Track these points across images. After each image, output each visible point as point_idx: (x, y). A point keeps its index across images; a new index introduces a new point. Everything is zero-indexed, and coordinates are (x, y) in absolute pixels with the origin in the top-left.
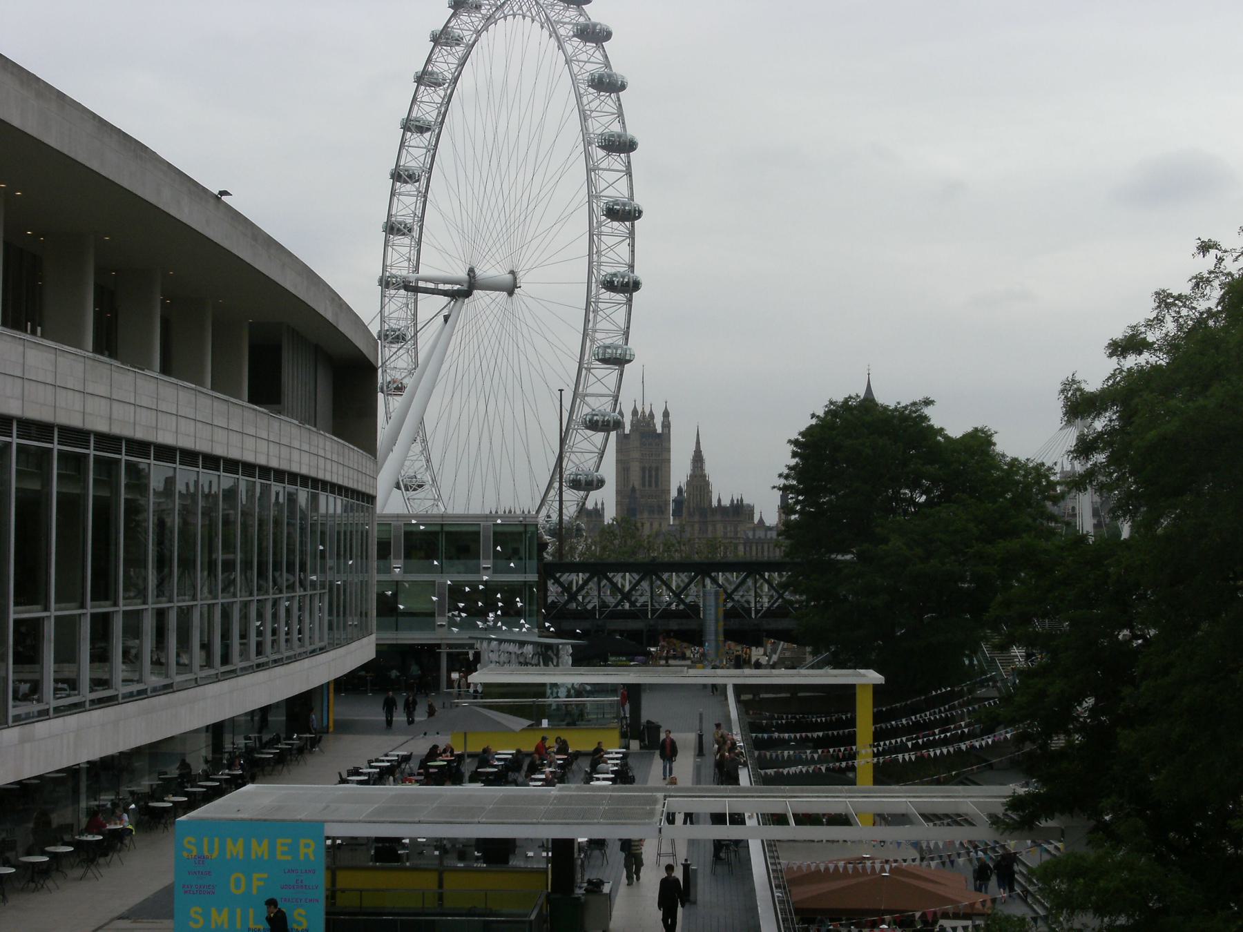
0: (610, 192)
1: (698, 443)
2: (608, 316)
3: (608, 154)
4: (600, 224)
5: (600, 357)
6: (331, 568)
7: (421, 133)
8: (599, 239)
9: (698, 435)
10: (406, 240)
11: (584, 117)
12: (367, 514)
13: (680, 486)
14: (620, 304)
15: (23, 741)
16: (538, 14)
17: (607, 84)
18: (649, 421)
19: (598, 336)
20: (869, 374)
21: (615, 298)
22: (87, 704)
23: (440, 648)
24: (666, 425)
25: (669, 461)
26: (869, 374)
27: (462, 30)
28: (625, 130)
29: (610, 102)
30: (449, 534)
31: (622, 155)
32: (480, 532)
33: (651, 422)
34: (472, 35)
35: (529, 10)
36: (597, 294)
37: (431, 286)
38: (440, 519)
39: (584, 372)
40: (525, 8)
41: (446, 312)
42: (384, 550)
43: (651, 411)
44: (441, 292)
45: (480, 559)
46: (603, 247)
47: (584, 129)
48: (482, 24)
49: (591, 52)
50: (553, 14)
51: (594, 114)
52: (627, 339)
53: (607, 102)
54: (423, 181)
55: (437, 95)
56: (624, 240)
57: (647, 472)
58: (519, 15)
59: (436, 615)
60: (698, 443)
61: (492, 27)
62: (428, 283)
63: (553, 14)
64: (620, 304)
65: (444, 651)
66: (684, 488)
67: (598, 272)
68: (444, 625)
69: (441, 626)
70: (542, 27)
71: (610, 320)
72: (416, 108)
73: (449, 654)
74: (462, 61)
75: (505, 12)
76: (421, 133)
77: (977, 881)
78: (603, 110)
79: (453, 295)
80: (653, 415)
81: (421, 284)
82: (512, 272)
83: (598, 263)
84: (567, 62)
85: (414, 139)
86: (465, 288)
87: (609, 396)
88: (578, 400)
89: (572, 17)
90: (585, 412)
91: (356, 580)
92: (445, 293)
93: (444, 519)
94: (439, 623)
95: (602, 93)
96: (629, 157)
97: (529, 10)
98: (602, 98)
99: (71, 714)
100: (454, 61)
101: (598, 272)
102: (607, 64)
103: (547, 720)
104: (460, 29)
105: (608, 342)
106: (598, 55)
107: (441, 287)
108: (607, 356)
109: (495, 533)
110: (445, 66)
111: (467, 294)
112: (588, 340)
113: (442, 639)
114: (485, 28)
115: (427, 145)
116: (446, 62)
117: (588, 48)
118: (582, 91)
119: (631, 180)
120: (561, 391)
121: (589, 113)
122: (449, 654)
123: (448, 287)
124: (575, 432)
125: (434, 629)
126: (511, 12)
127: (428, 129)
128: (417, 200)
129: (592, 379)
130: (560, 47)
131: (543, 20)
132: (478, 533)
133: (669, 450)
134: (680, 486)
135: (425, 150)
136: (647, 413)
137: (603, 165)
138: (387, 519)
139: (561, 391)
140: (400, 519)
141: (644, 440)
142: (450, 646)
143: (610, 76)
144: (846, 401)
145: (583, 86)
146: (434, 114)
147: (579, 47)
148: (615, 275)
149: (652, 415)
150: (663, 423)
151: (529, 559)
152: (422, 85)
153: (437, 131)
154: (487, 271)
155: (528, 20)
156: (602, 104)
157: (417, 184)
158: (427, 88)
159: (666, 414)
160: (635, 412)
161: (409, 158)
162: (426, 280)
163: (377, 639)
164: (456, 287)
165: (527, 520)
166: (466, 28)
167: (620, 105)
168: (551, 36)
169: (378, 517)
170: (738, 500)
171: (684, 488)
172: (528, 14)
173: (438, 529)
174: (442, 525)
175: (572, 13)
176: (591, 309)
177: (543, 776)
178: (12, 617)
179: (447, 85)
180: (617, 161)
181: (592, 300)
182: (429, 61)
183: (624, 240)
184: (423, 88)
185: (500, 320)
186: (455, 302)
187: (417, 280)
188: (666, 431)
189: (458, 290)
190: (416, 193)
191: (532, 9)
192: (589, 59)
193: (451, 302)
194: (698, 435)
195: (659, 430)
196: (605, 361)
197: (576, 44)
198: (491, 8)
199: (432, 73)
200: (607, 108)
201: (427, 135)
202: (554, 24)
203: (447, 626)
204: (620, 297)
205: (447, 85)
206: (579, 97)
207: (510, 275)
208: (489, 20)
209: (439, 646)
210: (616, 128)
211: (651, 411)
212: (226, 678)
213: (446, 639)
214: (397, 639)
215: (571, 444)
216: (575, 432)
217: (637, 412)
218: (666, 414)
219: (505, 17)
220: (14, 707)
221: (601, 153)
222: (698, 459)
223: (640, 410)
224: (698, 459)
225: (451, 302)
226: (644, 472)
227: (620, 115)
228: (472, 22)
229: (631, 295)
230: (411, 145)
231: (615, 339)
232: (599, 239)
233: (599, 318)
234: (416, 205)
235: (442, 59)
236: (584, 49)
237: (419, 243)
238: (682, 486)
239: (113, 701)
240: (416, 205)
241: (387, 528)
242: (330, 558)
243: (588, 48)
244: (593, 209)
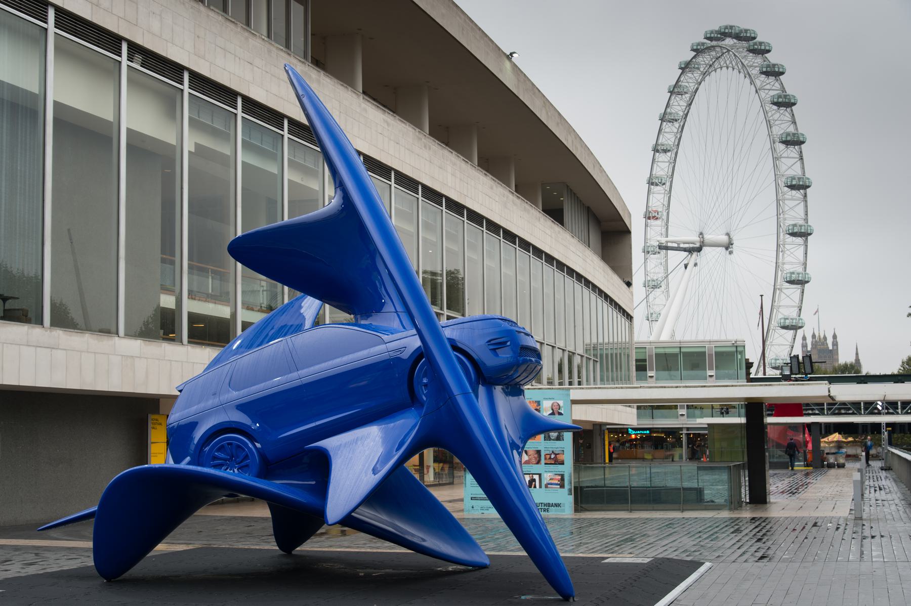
0: (791, 173)
2: (792, 253)
3: (787, 147)
4: (784, 194)
5: (788, 280)
7: (665, 152)
8: (784, 203)
9: (857, 349)
10: (658, 222)
11: (770, 125)
14: (800, 245)
16: (737, 64)
17: (785, 103)
18: (823, 342)
19: (786, 267)
21: (796, 241)
24: (835, 344)
27: (688, 82)
28: (797, 129)
29: (787, 114)
30: (686, 355)
31: (796, 147)
32: (706, 352)
33: (825, 342)
34: (695, 85)
35: (731, 62)
36: (784, 240)
37: (676, 245)
39: (778, 292)
40: (728, 62)
41: (686, 262)
42: (641, 367)
43: (825, 335)
44: (682, 249)
45: (706, 370)
46: (787, 208)
48: (701, 78)
50: (747, 62)
51: (777, 123)
52: (805, 268)
53: (784, 113)
54: (668, 184)
55: (673, 128)
56: (800, 203)
58: (725, 67)
59: (679, 408)
60: (857, 354)
61: (707, 78)
62: (673, 244)
63: (747, 62)
64: (800, 245)
67: (784, 225)
68: (684, 415)
69: (682, 415)
70: (740, 72)
71: (793, 256)
72: (661, 136)
73: (688, 435)
74: (689, 103)
75: (716, 67)
76: (665, 152)
79: (690, 251)
80: (826, 338)
81: (670, 245)
82: (728, 234)
83: (783, 218)
84: (757, 91)
85: (661, 157)
86: (698, 245)
87: (795, 307)
88: (775, 311)
90: (779, 317)
92: (685, 250)
93: (681, 344)
94: (681, 413)
96: (800, 148)
97: (731, 62)
98: (782, 112)
100: (684, 104)
101: (784, 225)
102: (783, 90)
103: (745, 422)
105: (792, 270)
106: (777, 85)
107: (682, 245)
108: (793, 279)
110: (679, 108)
111: (699, 250)
112: (779, 271)
113: (683, 424)
114: (703, 79)
115: (669, 159)
116: (679, 105)
118: (768, 109)
119: (803, 163)
120: (762, 296)
121: (772, 121)
122: (688, 435)
123: (686, 246)
124: (774, 331)
125: (678, 417)
126: (719, 66)
127: (669, 151)
128: (664, 196)
129: (783, 296)
130: (752, 82)
131: (740, 67)
135: (668, 164)
136: (822, 336)
137: (785, 155)
138: (644, 344)
139: (762, 296)
141: (821, 354)
143: (785, 96)
145: (768, 105)
148: (795, 225)
149: (825, 338)
150: (833, 342)
151: (740, 369)
152: (664, 121)
153: (675, 151)
154: (715, 235)
155: (730, 69)
156: (781, 116)
157: (664, 186)
158: (668, 123)
159: (835, 337)
160: (814, 336)
161: (658, 169)
162: (672, 242)
164: (691, 245)
165: (738, 343)
166: (691, 81)
167: (793, 115)
168: (745, 77)
169: (636, 343)
173: (677, 350)
174: (680, 347)
175: (759, 60)
176: (781, 250)
179: (680, 121)
180: (793, 151)
181: (781, 243)
182: (668, 105)
183: (800, 203)
184: (665, 123)
186: (691, 255)
187: (667, 242)
188: (836, 347)
189: (693, 248)
190: (663, 191)
192: (771, 88)
193: (688, 256)
194: (857, 349)
195: (831, 348)
196: (791, 282)
197: (762, 79)
198: (706, 66)
199: (670, 114)
200: (786, 118)
201: (669, 154)
202: (747, 67)
203: (686, 415)
204: (800, 240)
205: (680, 121)
206: (765, 113)
207: (727, 236)
208: (705, 74)
209: (681, 429)
210: (791, 129)
211: (825, 335)
212: (462, 303)
213: (686, 424)
215: (771, 340)
216: (774, 331)
217: (815, 336)
218: (835, 337)
219: (715, 70)
223: (817, 335)
225: (688, 256)
228: (694, 77)
229: (807, 239)
231: (797, 268)
232: (784, 203)
233: (785, 255)
234: (664, 199)
235: (676, 104)
237: (667, 225)
240: (664, 199)
241: (643, 350)
244: (779, 185)
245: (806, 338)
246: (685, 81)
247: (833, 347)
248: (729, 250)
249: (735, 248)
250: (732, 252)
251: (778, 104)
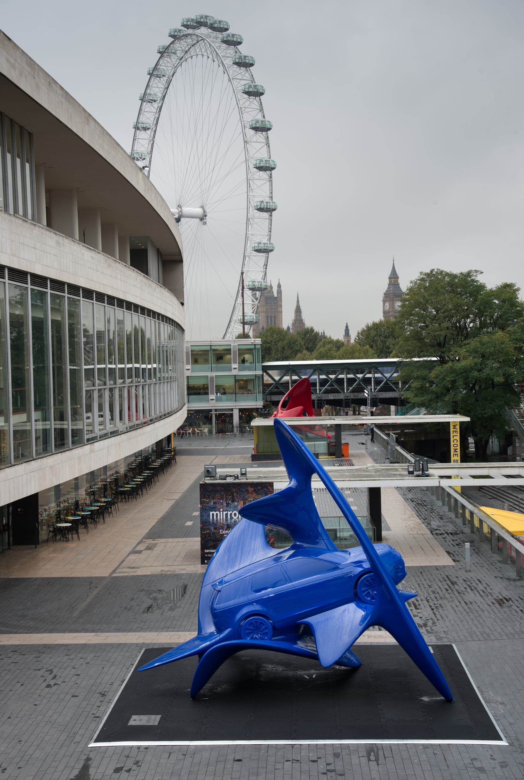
1: (298, 301)
6: (170, 370)
7: (145, 130)
9: (298, 297)
11: (241, 111)
12: (174, 341)
13: (288, 326)
15: (92, 451)
20: (393, 260)
22: (109, 434)
23: (211, 412)
24: (279, 292)
25: (281, 312)
26: (393, 260)
31: (264, 133)
38: (210, 343)
47: (241, 120)
49: (243, 74)
51: (247, 110)
57: (269, 318)
60: (298, 301)
65: (213, 413)
66: (291, 327)
69: (212, 399)
77: (224, 537)
78: (252, 107)
82: (202, 207)
84: (229, 80)
85: (141, 134)
89: (231, 53)
91: (167, 376)
93: (212, 343)
95: (251, 97)
96: (267, 134)
98: (251, 100)
99: (105, 439)
104: (165, 66)
109: (239, 350)
117: (242, 71)
121: (244, 109)
127: (148, 129)
132: (230, 350)
133: (281, 306)
134: (288, 326)
140: (188, 343)
142: (216, 410)
143: (255, 86)
144: (432, 271)
146: (152, 119)
147: (237, 71)
149: (271, 287)
150: (278, 291)
153: (154, 129)
159: (279, 286)
163: (187, 407)
170: (321, 333)
171: (291, 327)
172: (205, 54)
173: (208, 348)
175: (231, 51)
177: (114, 478)
178: (84, 389)
185: (195, 233)
188: (279, 295)
191: (208, 50)
194: (298, 297)
195: (276, 295)
201: (149, 132)
210: (259, 117)
213: (215, 406)
214: (256, 405)
218: (279, 286)
220: (87, 434)
221: (252, 132)
222: (298, 310)
224: (298, 310)
226: (268, 319)
227: (261, 110)
230: (140, 138)
236: (239, 72)
238: (290, 326)
239: (115, 433)
242: (170, 365)
243: (242, 71)
245: (280, 285)
246: (164, 65)
247: (277, 295)
248: (203, 221)
249: (208, 219)
250: (206, 223)
251: (249, 93)
